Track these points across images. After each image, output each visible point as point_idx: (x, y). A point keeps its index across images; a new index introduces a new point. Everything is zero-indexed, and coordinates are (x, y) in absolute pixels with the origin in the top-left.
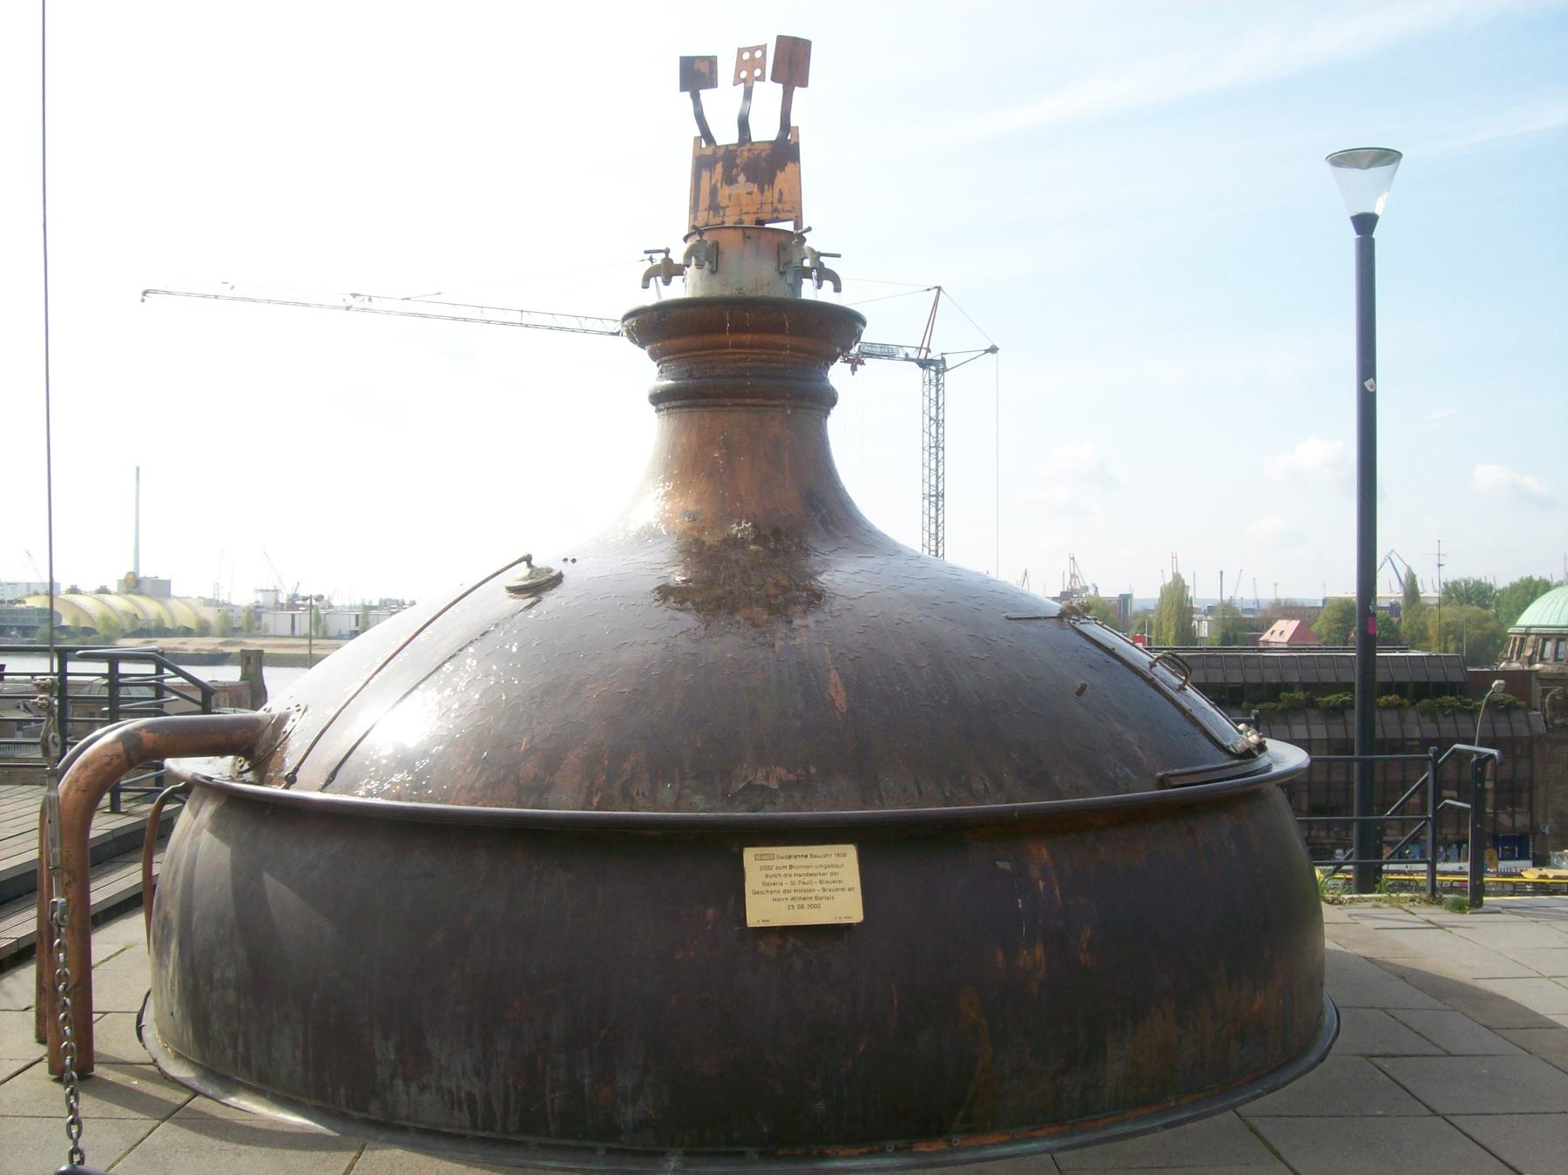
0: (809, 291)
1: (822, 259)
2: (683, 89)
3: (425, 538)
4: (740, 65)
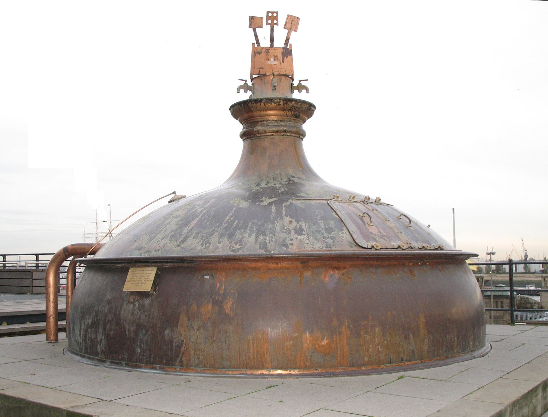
0: (296, 95)
1: (301, 82)
3: (124, 161)
4: (268, 18)
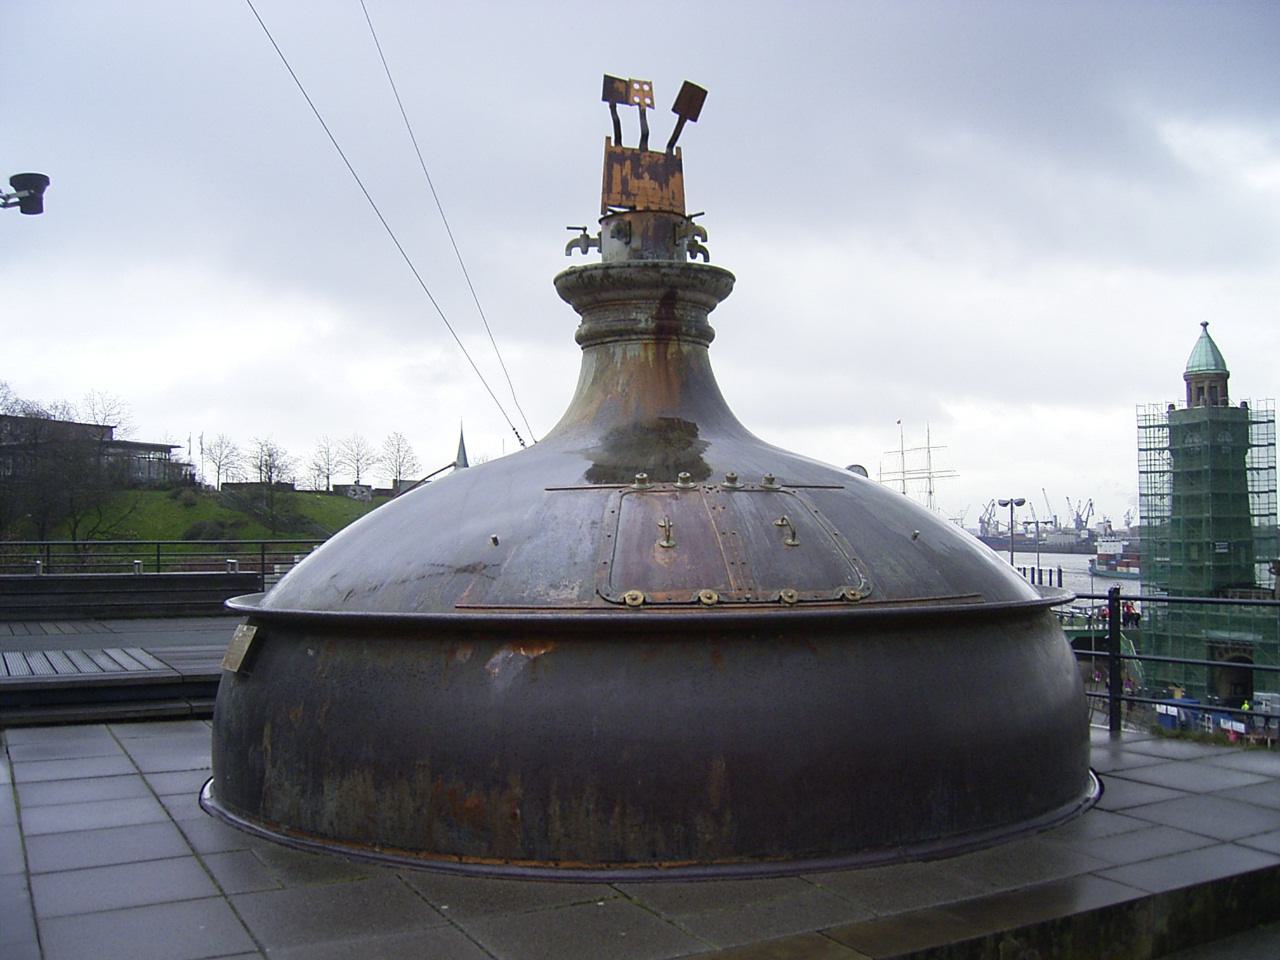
2: (604, 99)
